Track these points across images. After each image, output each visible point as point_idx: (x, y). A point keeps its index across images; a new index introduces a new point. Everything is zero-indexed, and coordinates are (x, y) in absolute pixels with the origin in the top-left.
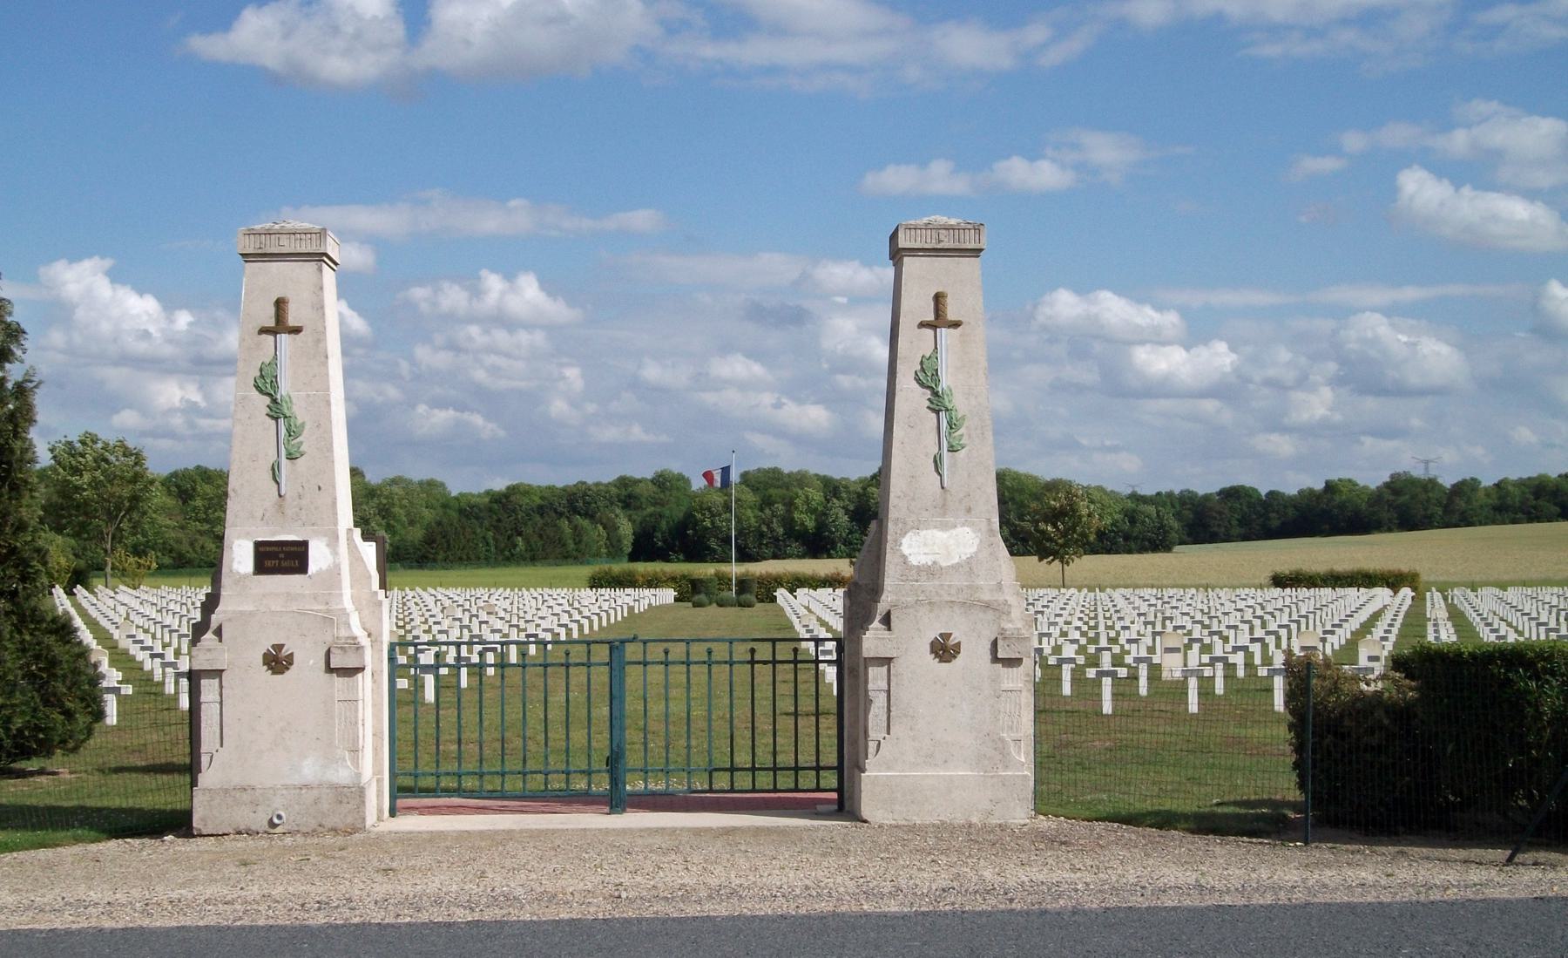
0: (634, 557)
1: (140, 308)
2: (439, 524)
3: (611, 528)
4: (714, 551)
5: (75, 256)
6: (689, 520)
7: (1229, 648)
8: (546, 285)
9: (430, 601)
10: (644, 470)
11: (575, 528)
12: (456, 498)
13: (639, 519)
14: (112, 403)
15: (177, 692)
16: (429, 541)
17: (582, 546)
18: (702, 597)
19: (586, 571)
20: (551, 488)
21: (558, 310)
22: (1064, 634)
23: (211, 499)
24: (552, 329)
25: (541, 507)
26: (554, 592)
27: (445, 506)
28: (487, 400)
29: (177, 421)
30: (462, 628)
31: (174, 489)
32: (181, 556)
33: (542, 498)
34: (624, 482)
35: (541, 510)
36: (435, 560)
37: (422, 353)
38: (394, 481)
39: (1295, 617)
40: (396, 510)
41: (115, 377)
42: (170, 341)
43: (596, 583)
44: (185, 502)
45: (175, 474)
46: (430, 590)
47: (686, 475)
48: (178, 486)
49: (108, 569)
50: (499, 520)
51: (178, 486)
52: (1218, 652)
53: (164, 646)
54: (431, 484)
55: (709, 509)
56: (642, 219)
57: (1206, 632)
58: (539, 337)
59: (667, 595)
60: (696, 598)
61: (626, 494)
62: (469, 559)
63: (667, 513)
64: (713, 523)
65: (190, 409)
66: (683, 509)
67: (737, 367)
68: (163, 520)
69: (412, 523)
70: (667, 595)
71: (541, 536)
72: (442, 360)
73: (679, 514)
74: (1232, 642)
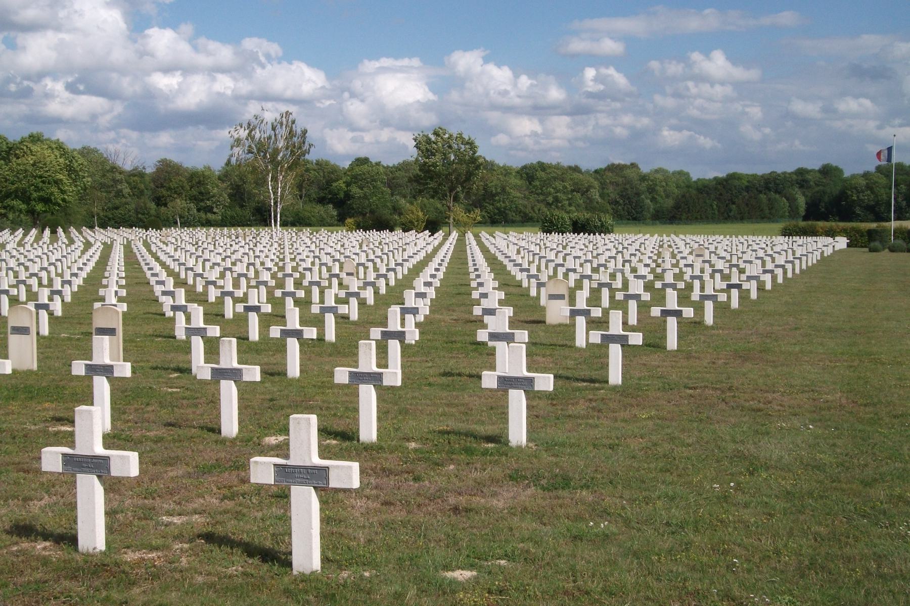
0: (806, 218)
1: (500, 76)
2: (683, 196)
3: (792, 200)
4: (859, 215)
5: (467, 47)
6: (843, 195)
7: (744, 277)
8: (733, 59)
9: (681, 244)
10: (814, 164)
11: (769, 200)
12: (695, 182)
13: (809, 194)
14: (492, 131)
15: (529, 287)
16: (677, 207)
17: (773, 211)
18: (877, 244)
19: (780, 226)
20: (754, 176)
21: (739, 73)
22: (262, 264)
23: (545, 181)
24: (738, 85)
25: (747, 187)
26: (758, 239)
27: (688, 187)
28: (701, 125)
29: (528, 141)
30: (315, 257)
31: (524, 175)
32: (526, 215)
33: (748, 182)
34: (801, 172)
35: (747, 189)
36: (680, 219)
37: (659, 99)
38: (657, 171)
39: (791, 258)
40: (658, 188)
41: (494, 117)
42: (519, 97)
43: (787, 233)
44: (530, 184)
45: (525, 167)
46: (682, 236)
47: (841, 167)
48: (527, 174)
49: (451, 220)
50: (721, 194)
51: (527, 174)
52: (735, 280)
53: (530, 263)
54: (681, 173)
55: (856, 188)
56: (787, 18)
57: (727, 265)
58: (729, 90)
59: (842, 242)
60: (872, 244)
61: (801, 177)
62: (701, 218)
63: (829, 191)
64: (858, 197)
65: (534, 134)
66: (839, 188)
67: (851, 105)
68: (515, 193)
69: (668, 196)
70: (842, 242)
71: (747, 205)
72: (669, 103)
73: (835, 190)
74: (748, 273)
